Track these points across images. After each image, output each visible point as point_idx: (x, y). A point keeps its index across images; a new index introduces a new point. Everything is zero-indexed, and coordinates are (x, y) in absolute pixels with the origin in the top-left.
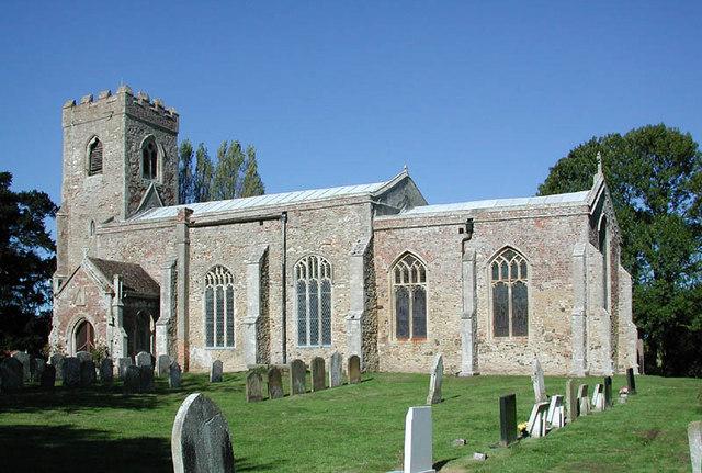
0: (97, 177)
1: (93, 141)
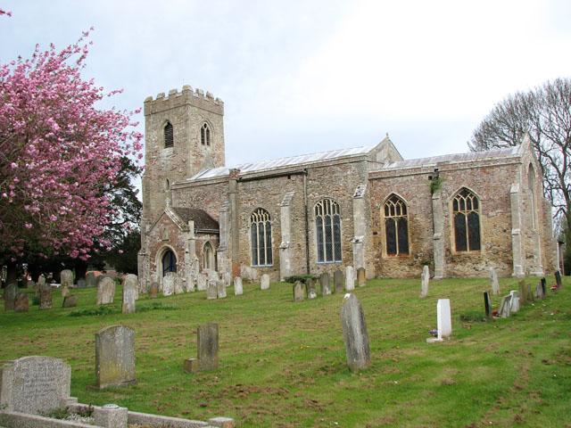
0: (168, 151)
1: (166, 124)
